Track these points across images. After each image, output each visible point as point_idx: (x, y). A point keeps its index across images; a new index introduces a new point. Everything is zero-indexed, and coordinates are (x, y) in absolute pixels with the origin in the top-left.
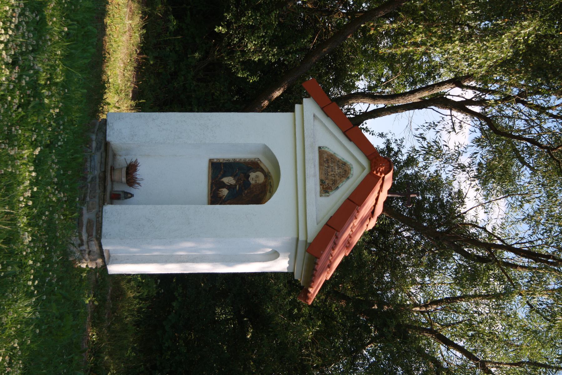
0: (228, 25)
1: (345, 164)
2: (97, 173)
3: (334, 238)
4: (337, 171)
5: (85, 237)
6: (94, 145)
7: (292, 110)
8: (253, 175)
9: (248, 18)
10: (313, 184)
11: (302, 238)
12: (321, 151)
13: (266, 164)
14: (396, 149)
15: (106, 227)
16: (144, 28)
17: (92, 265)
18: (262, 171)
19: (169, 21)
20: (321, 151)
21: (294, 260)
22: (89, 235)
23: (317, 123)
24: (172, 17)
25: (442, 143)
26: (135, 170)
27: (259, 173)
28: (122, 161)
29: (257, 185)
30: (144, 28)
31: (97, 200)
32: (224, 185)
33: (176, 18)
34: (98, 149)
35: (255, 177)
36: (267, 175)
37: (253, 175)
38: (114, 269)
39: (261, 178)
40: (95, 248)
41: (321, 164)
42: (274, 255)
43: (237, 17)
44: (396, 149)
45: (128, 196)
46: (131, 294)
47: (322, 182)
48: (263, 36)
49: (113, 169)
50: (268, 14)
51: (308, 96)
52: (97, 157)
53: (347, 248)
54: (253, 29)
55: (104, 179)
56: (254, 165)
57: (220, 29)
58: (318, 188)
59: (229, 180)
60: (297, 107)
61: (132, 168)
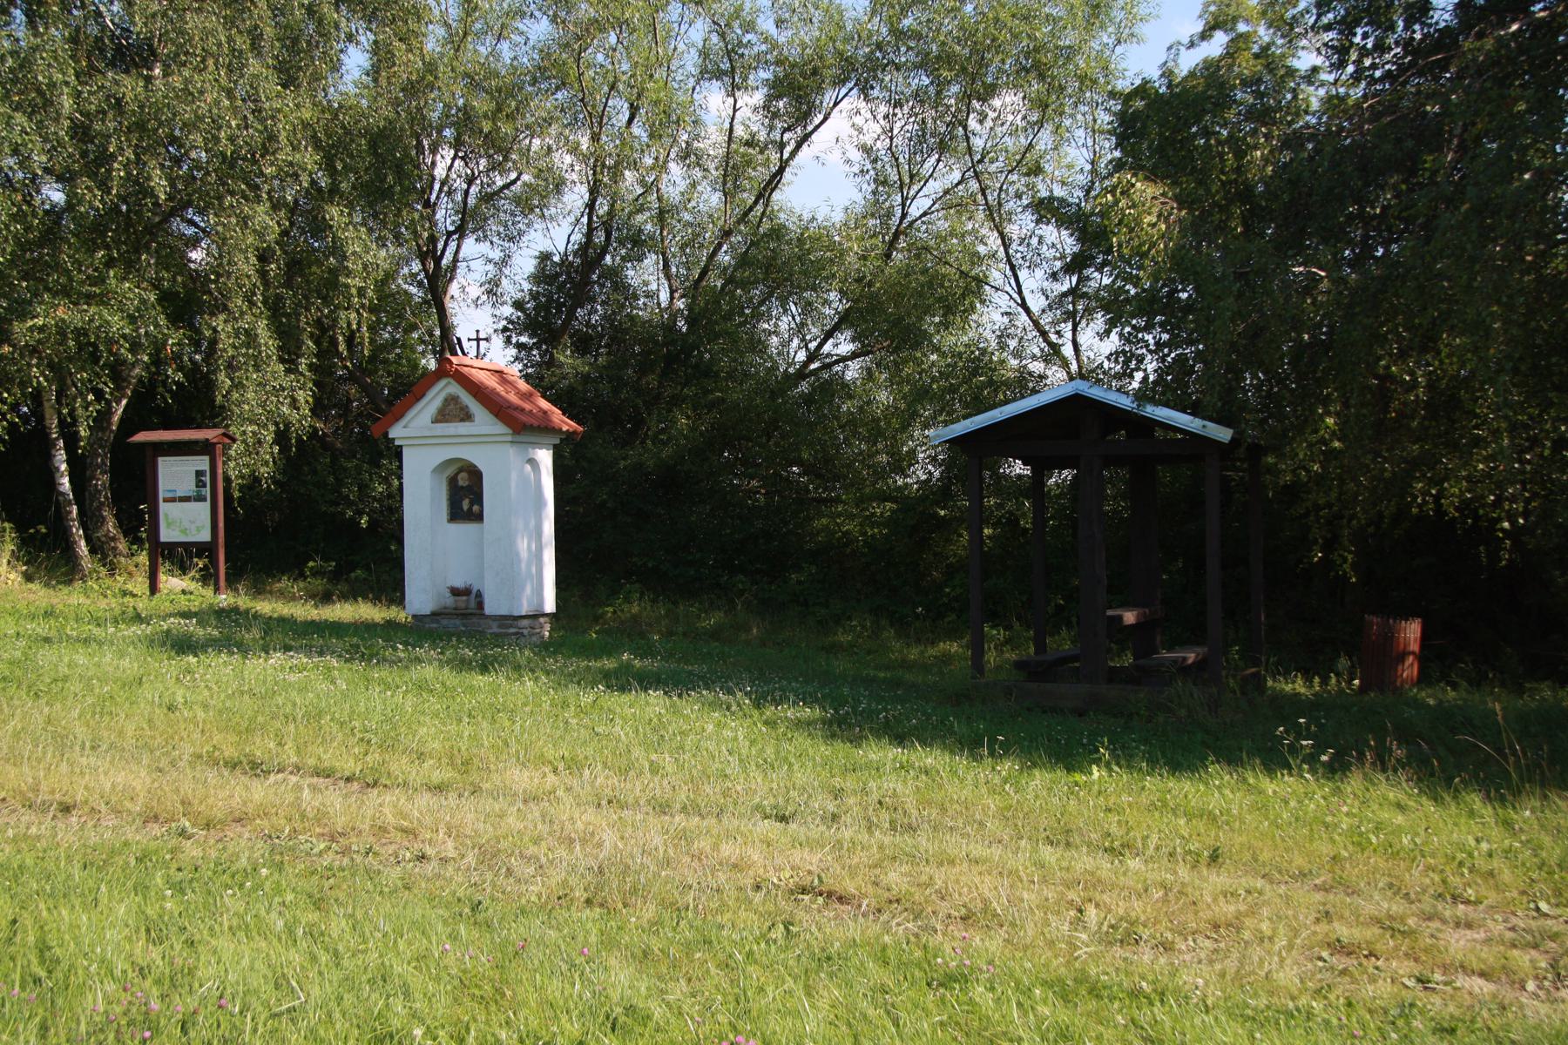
0: (360, 513)
1: (446, 400)
2: (458, 622)
3: (510, 411)
4: (452, 407)
5: (512, 630)
6: (434, 625)
7: (401, 447)
8: (461, 483)
9: (352, 492)
10: (462, 428)
11: (509, 438)
12: (435, 421)
13: (450, 471)
14: (505, 323)
15: (504, 612)
16: (356, 601)
17: (548, 627)
18: (457, 474)
19: (356, 578)
20: (435, 421)
21: (541, 446)
22: (511, 626)
23: (411, 425)
24: (353, 575)
25: (484, 279)
26: (458, 589)
27: (459, 477)
28: (450, 601)
29: (470, 479)
30: (356, 601)
31: (482, 621)
32: (470, 509)
33: (353, 570)
34: (438, 622)
35: (463, 480)
36: (461, 470)
37: (461, 483)
38: (550, 606)
39: (463, 475)
40: (525, 622)
41: (447, 422)
42: (532, 462)
43: (350, 504)
44: (505, 323)
45: (479, 595)
46: (635, 609)
47: (462, 420)
48: (370, 475)
49: (456, 609)
50: (345, 470)
51: (387, 433)
52: (445, 622)
53: (531, 395)
54: (363, 488)
55: (464, 616)
56: (452, 482)
57: (364, 521)
58: (467, 424)
59: (465, 505)
60: (397, 443)
61: (455, 592)
